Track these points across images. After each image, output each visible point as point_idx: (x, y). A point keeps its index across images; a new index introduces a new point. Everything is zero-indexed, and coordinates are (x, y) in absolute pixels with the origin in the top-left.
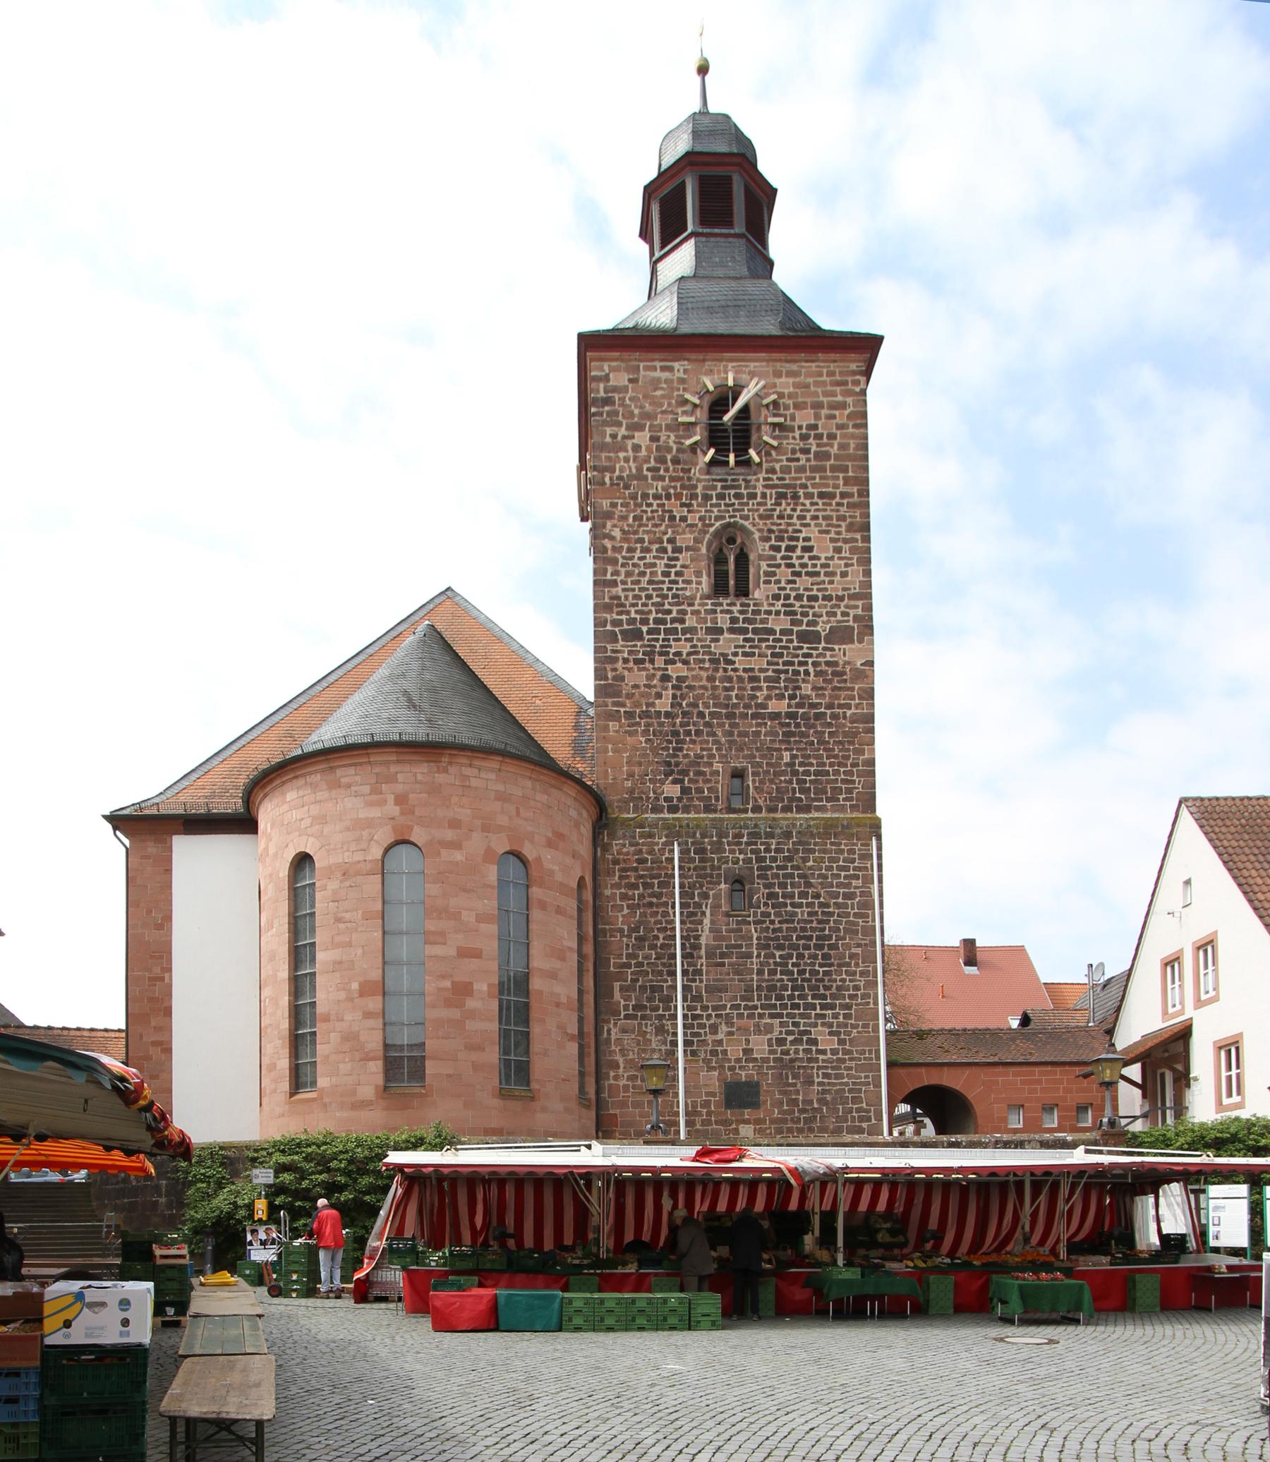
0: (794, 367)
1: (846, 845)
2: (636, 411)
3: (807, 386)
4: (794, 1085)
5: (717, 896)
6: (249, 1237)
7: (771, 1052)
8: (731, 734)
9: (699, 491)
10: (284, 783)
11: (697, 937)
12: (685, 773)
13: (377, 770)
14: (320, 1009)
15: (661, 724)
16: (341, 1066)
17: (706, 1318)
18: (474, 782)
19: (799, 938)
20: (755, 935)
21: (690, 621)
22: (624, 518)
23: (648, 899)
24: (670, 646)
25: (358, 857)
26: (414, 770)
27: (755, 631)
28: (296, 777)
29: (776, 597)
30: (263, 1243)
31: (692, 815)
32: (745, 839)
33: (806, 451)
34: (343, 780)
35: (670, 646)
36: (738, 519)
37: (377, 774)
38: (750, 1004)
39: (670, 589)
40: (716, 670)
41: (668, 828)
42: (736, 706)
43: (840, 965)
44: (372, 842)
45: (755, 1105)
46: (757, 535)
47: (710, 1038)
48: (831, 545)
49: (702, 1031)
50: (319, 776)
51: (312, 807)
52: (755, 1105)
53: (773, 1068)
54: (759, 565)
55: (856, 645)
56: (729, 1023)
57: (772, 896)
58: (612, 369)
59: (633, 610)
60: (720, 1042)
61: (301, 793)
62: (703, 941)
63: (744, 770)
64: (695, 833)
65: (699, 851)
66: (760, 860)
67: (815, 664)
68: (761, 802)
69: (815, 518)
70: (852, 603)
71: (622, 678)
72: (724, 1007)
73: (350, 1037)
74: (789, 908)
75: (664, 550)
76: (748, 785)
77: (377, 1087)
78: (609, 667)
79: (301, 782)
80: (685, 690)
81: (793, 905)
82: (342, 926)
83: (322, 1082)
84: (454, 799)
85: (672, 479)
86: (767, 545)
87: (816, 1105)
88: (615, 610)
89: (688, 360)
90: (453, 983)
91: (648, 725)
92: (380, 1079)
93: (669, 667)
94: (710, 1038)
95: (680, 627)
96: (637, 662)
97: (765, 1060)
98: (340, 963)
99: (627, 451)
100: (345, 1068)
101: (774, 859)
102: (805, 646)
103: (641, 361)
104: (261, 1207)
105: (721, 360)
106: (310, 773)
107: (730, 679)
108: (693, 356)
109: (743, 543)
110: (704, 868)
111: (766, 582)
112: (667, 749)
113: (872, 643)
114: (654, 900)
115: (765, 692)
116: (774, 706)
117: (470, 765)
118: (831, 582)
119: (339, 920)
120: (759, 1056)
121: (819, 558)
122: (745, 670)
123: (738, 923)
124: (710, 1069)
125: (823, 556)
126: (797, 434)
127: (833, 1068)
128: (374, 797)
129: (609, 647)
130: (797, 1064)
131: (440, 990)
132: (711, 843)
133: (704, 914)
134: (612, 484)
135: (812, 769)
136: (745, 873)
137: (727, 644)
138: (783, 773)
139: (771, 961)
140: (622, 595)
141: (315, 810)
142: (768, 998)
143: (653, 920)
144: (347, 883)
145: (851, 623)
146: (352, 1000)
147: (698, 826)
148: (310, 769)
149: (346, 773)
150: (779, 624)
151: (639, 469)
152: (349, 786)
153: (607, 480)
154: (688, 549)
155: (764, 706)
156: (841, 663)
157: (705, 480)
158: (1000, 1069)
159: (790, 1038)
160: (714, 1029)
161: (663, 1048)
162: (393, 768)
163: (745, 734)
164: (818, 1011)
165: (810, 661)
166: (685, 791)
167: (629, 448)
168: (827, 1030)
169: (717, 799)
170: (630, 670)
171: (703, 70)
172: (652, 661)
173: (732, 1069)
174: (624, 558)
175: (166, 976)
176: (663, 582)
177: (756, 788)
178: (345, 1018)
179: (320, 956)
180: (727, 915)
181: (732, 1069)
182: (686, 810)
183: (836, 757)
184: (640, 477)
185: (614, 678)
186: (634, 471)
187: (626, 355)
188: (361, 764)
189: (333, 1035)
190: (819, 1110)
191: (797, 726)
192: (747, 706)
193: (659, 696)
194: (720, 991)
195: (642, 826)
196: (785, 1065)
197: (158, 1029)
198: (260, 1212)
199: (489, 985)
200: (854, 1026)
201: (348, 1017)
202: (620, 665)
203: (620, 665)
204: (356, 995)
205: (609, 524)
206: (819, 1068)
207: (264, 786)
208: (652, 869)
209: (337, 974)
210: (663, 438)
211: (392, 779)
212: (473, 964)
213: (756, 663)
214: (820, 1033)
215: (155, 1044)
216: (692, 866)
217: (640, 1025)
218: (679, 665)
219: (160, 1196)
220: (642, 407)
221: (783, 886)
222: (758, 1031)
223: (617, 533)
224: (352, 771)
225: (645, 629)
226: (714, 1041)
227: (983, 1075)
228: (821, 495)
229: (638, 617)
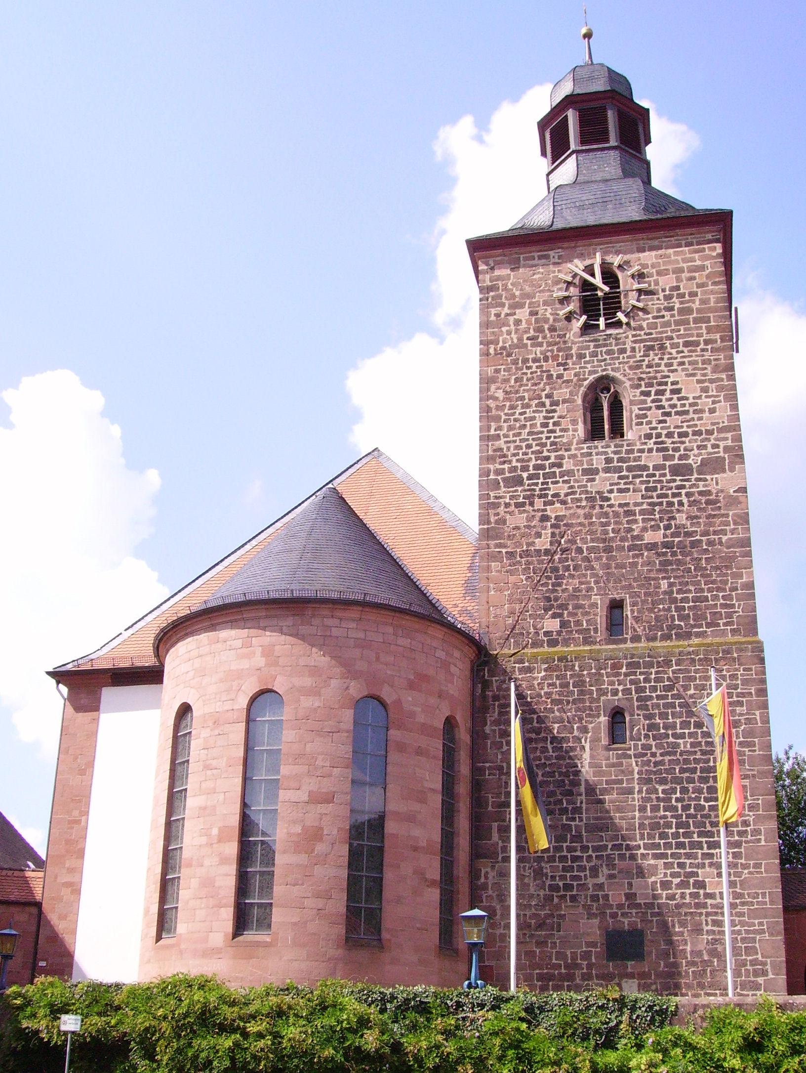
2: (517, 293)
5: (597, 729)
12: (563, 607)
19: (682, 771)
20: (636, 769)
22: (506, 381)
24: (549, 489)
25: (228, 706)
27: (629, 469)
29: (648, 436)
31: (572, 648)
32: (624, 670)
40: (593, 507)
47: (590, 882)
49: (582, 874)
52: (639, 955)
59: (514, 459)
60: (600, 887)
64: (574, 666)
74: (671, 739)
80: (563, 528)
81: (675, 736)
82: (209, 772)
88: (498, 460)
96: (517, 505)
98: (205, 808)
101: (654, 689)
102: (678, 478)
105: (590, 245)
107: (606, 515)
108: (566, 245)
113: (743, 470)
116: (657, 537)
120: (642, 902)
123: (619, 757)
124: (591, 916)
125: (691, 396)
130: (683, 910)
133: (583, 748)
134: (496, 354)
135: (690, 596)
137: (602, 482)
139: (654, 796)
151: (520, 339)
156: (714, 491)
157: (579, 342)
159: (676, 881)
160: (594, 871)
161: (542, 893)
164: (706, 851)
165: (683, 491)
166: (564, 624)
173: (614, 916)
174: (506, 414)
175: (83, 818)
181: (614, 916)
182: (566, 643)
184: (521, 345)
190: (708, 963)
191: (674, 554)
192: (623, 539)
194: (601, 830)
201: (207, 862)
213: (631, 498)
218: (558, 505)
221: (664, 716)
228: (686, 344)
229: (519, 465)
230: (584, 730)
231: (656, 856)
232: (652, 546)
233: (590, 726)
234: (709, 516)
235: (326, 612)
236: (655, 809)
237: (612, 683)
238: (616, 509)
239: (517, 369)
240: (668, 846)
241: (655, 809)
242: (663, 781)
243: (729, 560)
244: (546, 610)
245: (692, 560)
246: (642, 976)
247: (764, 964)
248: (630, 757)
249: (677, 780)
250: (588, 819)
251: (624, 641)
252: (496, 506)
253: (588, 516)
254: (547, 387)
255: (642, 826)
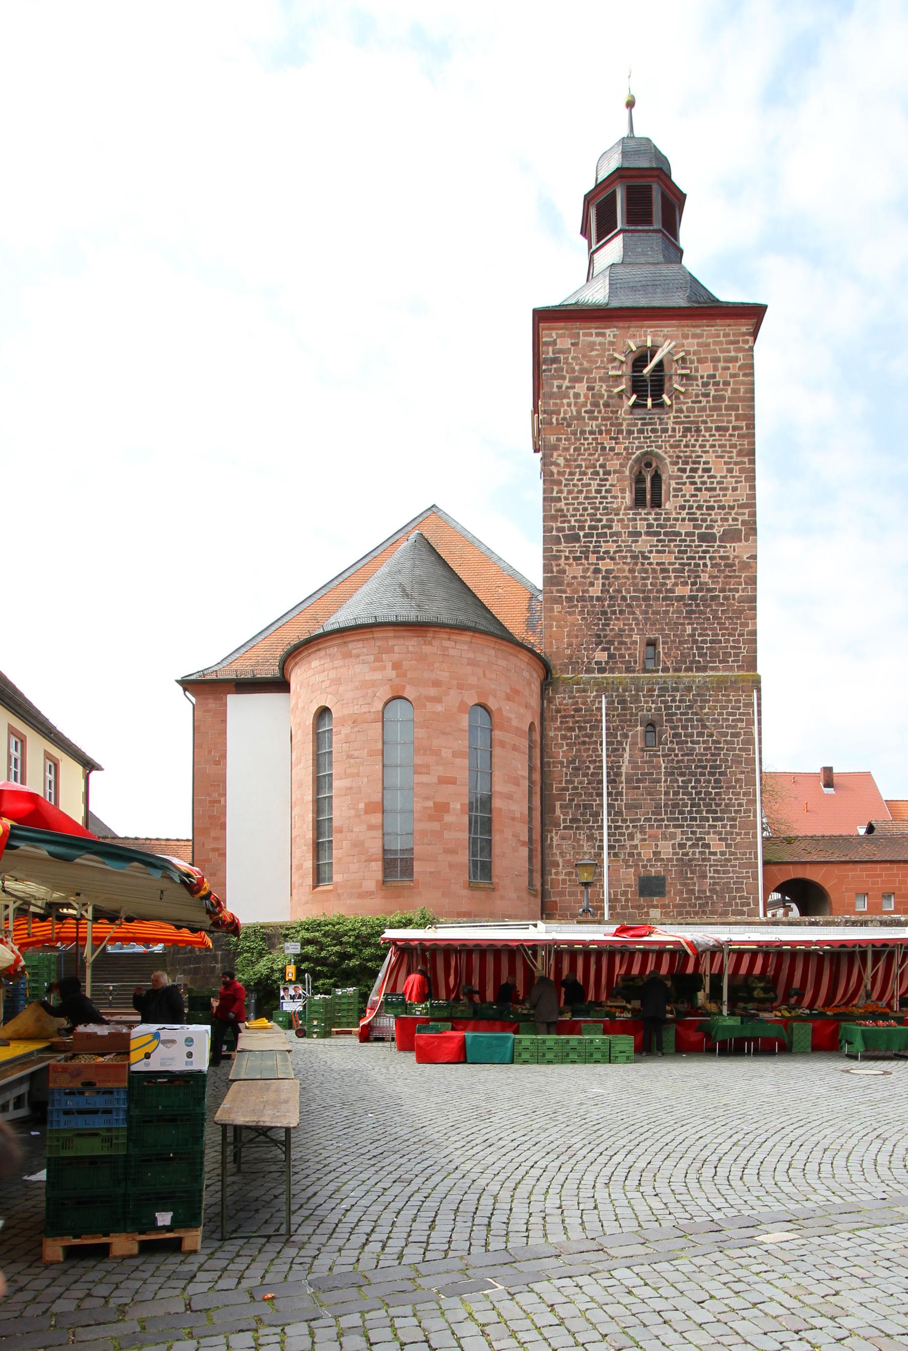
0: (698, 331)
1: (733, 696)
2: (577, 368)
3: (708, 345)
4: (692, 879)
5: (635, 736)
6: (282, 994)
7: (674, 854)
8: (646, 612)
9: (624, 427)
10: (310, 654)
11: (619, 767)
12: (611, 642)
13: (379, 643)
14: (335, 823)
15: (593, 606)
16: (351, 866)
17: (623, 1054)
18: (451, 652)
19: (697, 767)
21: (616, 527)
22: (567, 449)
23: (582, 739)
24: (601, 547)
25: (365, 709)
26: (407, 644)
28: (319, 650)
29: (682, 508)
30: (292, 998)
32: (656, 693)
33: (706, 395)
34: (353, 652)
35: (601, 547)
36: (654, 448)
37: (379, 646)
38: (659, 817)
39: (601, 503)
40: (636, 564)
41: (598, 685)
42: (650, 591)
43: (728, 788)
44: (375, 698)
45: (662, 894)
46: (668, 461)
47: (628, 843)
48: (725, 467)
50: (336, 649)
51: (331, 672)
52: (662, 894)
53: (676, 865)
54: (669, 483)
55: (744, 543)
56: (643, 832)
57: (676, 735)
58: (558, 336)
59: (573, 519)
60: (636, 847)
61: (322, 662)
62: (624, 770)
63: (656, 640)
64: (618, 689)
65: (622, 702)
66: (668, 708)
67: (711, 558)
68: (669, 664)
69: (713, 446)
70: (741, 511)
71: (564, 572)
72: (639, 820)
73: (358, 844)
74: (689, 745)
75: (597, 474)
76: (659, 652)
77: (377, 881)
78: (554, 563)
79: (322, 653)
80: (612, 580)
81: (692, 742)
82: (352, 761)
83: (337, 878)
84: (436, 665)
85: (604, 419)
86: (676, 468)
87: (708, 894)
88: (559, 519)
89: (617, 327)
90: (435, 803)
91: (583, 607)
92: (379, 876)
93: (600, 562)
94: (628, 843)
95: (608, 532)
96: (575, 559)
97: (671, 860)
98: (351, 788)
99: (569, 398)
100: (354, 867)
102: (704, 544)
103: (580, 329)
104: (291, 971)
105: (642, 327)
106: (330, 647)
107: (646, 571)
108: (621, 324)
109: (657, 466)
110: (625, 715)
111: (674, 496)
112: (597, 625)
113: (755, 541)
114: (587, 739)
115: (673, 580)
117: (449, 639)
118: (725, 495)
119: (350, 757)
120: (665, 857)
121: (715, 477)
122: (658, 564)
123: (650, 756)
124: (628, 866)
125: (718, 475)
126: (700, 382)
127: (721, 866)
128: (377, 664)
129: (555, 548)
130: (694, 863)
131: (425, 808)
132: (631, 696)
133: (624, 749)
134: (558, 424)
136: (656, 718)
137: (644, 544)
138: (686, 642)
139: (675, 785)
140: (565, 508)
141: (333, 674)
142: (672, 813)
143: (586, 754)
144: (356, 729)
145: (740, 527)
146: (359, 816)
147: (620, 683)
148: (329, 644)
149: (356, 646)
150: (684, 528)
151: (579, 412)
152: (358, 656)
153: (554, 420)
154: (615, 472)
155: (672, 591)
156: (731, 557)
157: (629, 419)
158: (850, 866)
159: (689, 843)
160: (631, 837)
161: (593, 851)
162: (391, 642)
163: (658, 613)
164: (711, 823)
165: (708, 556)
166: (611, 656)
167: (571, 396)
168: (718, 837)
169: (635, 662)
170: (570, 565)
171: (630, 104)
172: (587, 558)
174: (566, 480)
175: (222, 799)
176: (596, 498)
177: (665, 654)
178: (355, 830)
179: (336, 784)
180: (642, 750)
181: (645, 866)
182: (612, 671)
183: (727, 629)
184: (579, 417)
185: (558, 572)
186: (575, 413)
187: (569, 325)
188: (367, 639)
189: (344, 842)
191: (697, 605)
192: (659, 591)
193: (592, 584)
194: (636, 808)
195: (578, 684)
196: (685, 864)
197: (216, 839)
198: (290, 975)
199: (462, 805)
200: (738, 834)
201: (356, 829)
202: (562, 561)
203: (562, 561)
204: (363, 813)
205: (555, 454)
206: (711, 866)
207: (295, 657)
208: (586, 716)
209: (349, 797)
210: (597, 388)
211: (390, 650)
212: (451, 788)
213: (666, 558)
214: (712, 839)
215: (214, 850)
216: (616, 713)
217: (575, 834)
218: (608, 561)
219: (217, 963)
220: (581, 364)
221: (685, 728)
222: (665, 838)
223: (561, 461)
224: (360, 644)
225: (582, 534)
226: (631, 846)
227: (836, 870)
228: (718, 429)
230: (626, 736)
231: (675, 826)
232: (681, 598)
233: (630, 734)
234: (726, 577)
235: (445, 636)
236: (676, 793)
237: (646, 702)
238: (655, 566)
239: (576, 439)
240: (685, 819)
241: (676, 793)
242: (682, 774)
243: (741, 612)
244: (597, 644)
245: (711, 610)
246: (664, 906)
247: (748, 898)
248: (659, 756)
249: (693, 774)
250: (627, 800)
251: (657, 671)
252: (559, 558)
253: (632, 571)
254: (601, 458)
255: (666, 805)
